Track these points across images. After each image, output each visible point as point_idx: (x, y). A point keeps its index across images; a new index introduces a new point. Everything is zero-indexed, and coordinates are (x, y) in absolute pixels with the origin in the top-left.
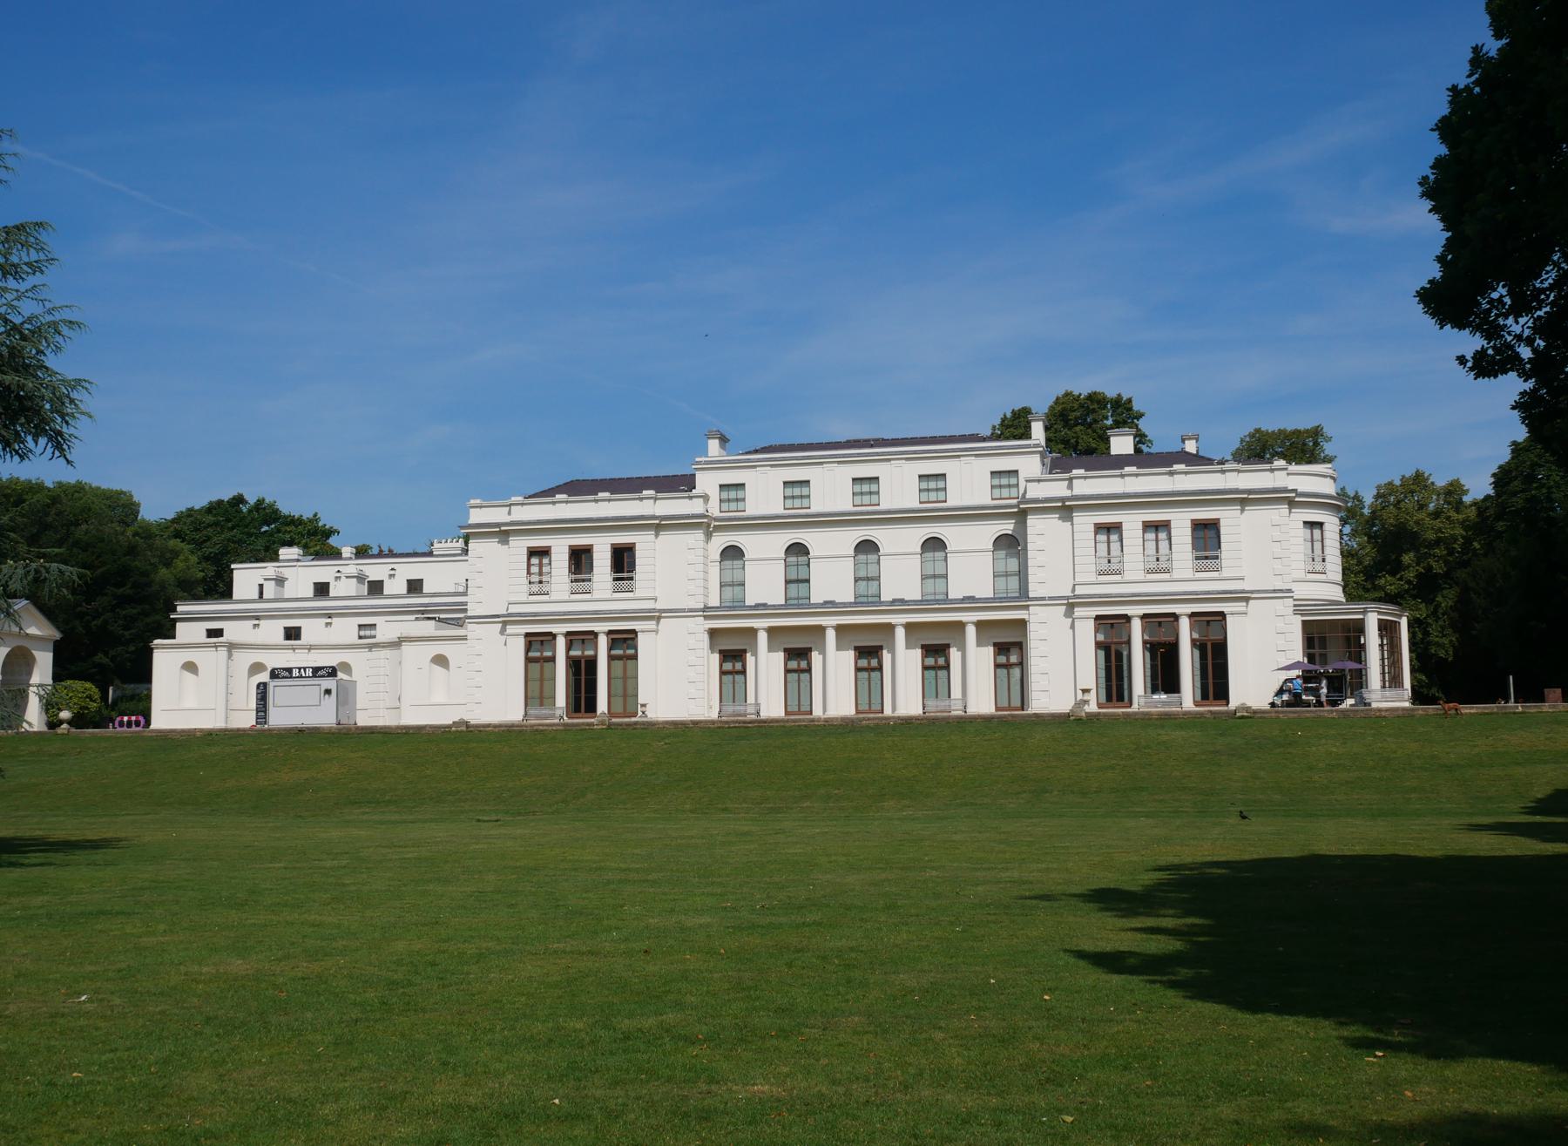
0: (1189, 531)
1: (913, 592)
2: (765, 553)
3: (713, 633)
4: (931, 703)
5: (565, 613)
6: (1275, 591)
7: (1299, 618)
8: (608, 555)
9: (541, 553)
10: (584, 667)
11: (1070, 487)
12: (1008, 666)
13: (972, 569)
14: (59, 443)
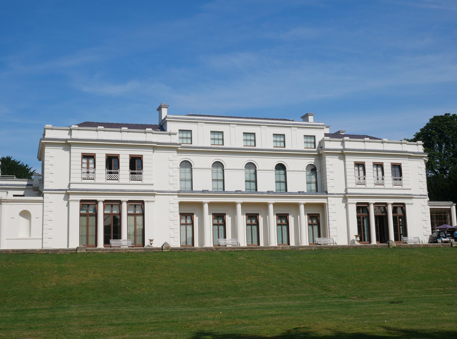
0: (390, 168)
1: (209, 186)
4: (317, 240)
5: (105, 190)
6: (421, 195)
7: (429, 207)
8: (104, 160)
9: (91, 157)
10: (108, 219)
11: (70, 134)
12: (186, 224)
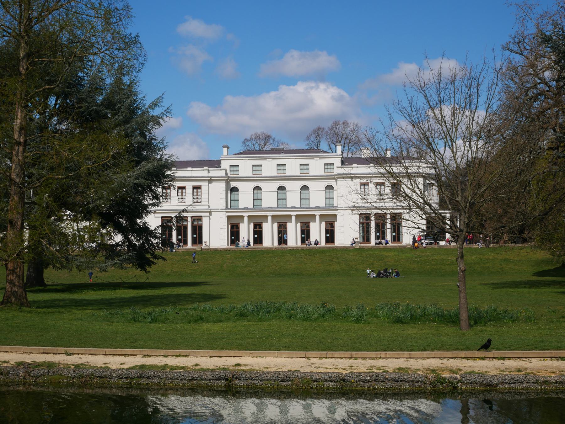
3: (228, 217)
13: (317, 198)
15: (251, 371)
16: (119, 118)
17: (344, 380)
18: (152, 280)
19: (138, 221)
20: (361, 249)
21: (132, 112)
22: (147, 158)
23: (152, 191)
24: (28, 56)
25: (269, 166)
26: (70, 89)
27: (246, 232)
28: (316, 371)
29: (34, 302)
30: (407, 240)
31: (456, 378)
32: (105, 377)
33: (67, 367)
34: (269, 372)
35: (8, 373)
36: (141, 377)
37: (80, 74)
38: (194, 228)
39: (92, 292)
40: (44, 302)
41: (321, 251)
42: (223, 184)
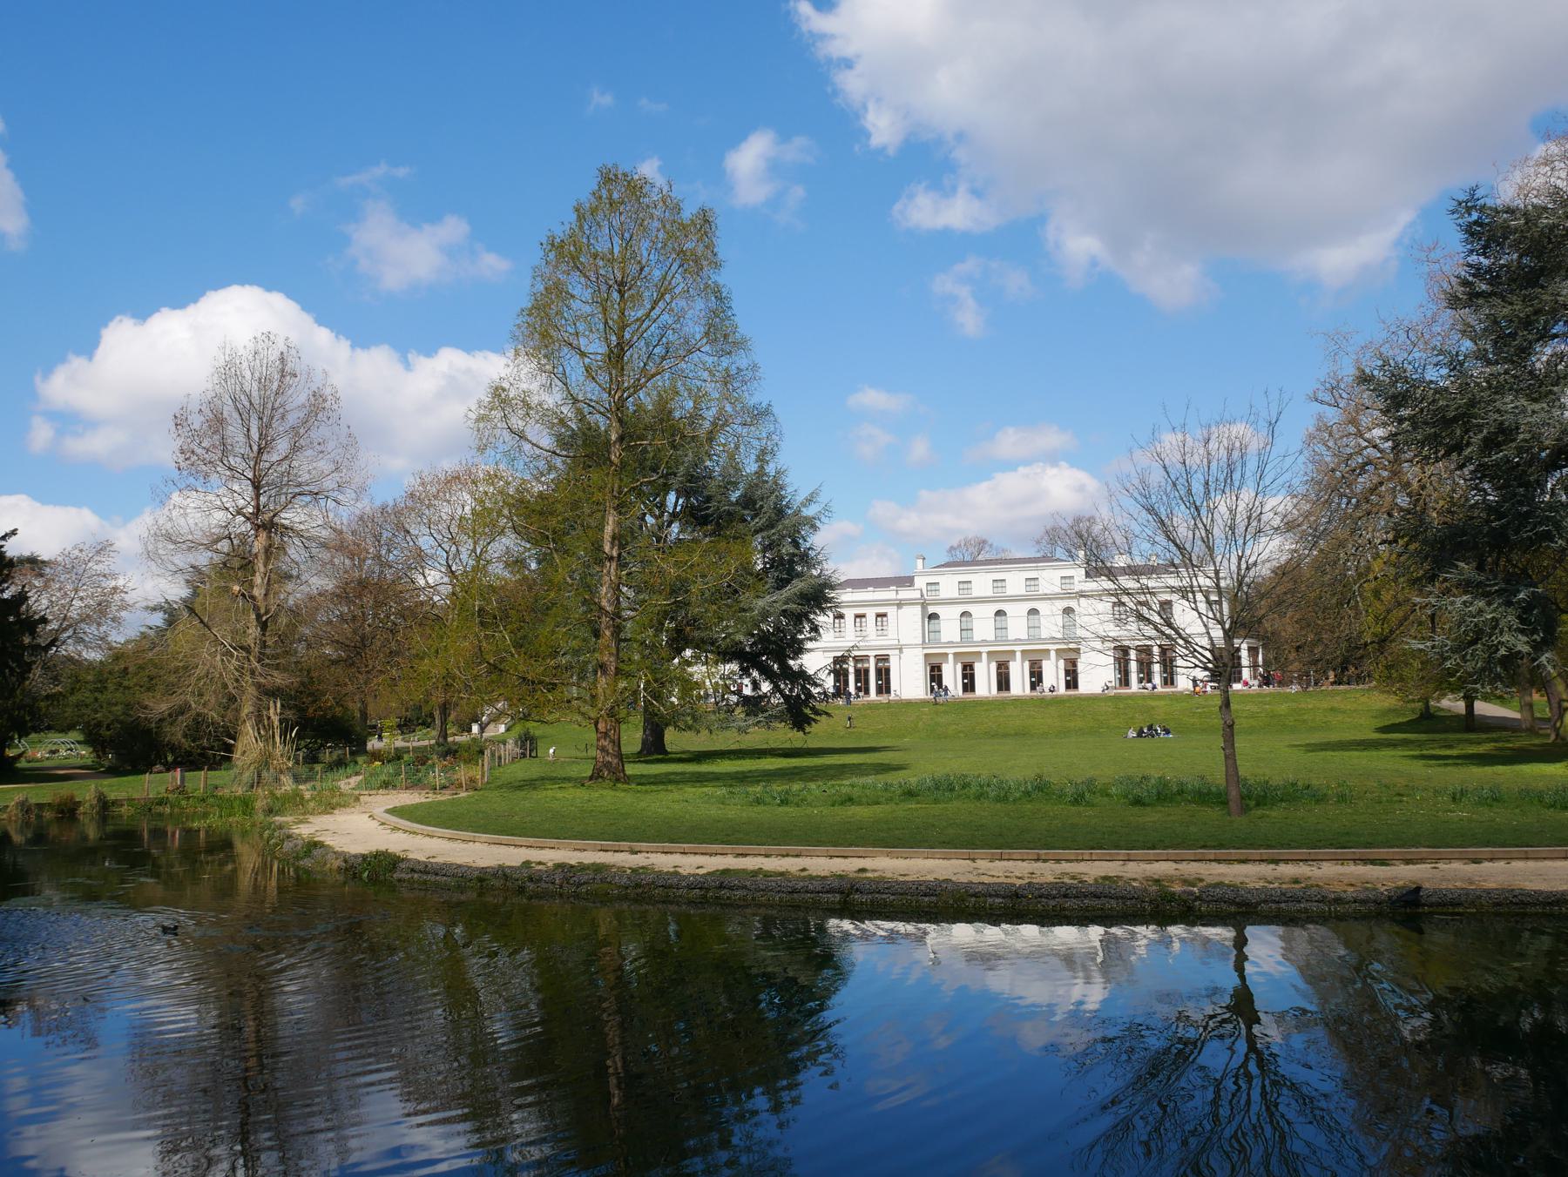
2: (949, 619)
3: (926, 655)
14: (1320, 418)
15: (881, 880)
16: (759, 522)
17: (1017, 895)
18: (813, 744)
19: (791, 662)
20: (1117, 698)
21: (780, 512)
22: (800, 575)
23: (810, 621)
24: (621, 439)
25: (982, 582)
26: (693, 485)
27: (952, 677)
28: (975, 880)
29: (635, 776)
30: (1183, 683)
31: (1192, 893)
32: (671, 887)
33: (622, 869)
34: (905, 882)
35: (540, 880)
36: (721, 887)
37: (708, 463)
38: (879, 671)
39: (727, 762)
40: (655, 776)
41: (1059, 701)
42: (919, 608)
